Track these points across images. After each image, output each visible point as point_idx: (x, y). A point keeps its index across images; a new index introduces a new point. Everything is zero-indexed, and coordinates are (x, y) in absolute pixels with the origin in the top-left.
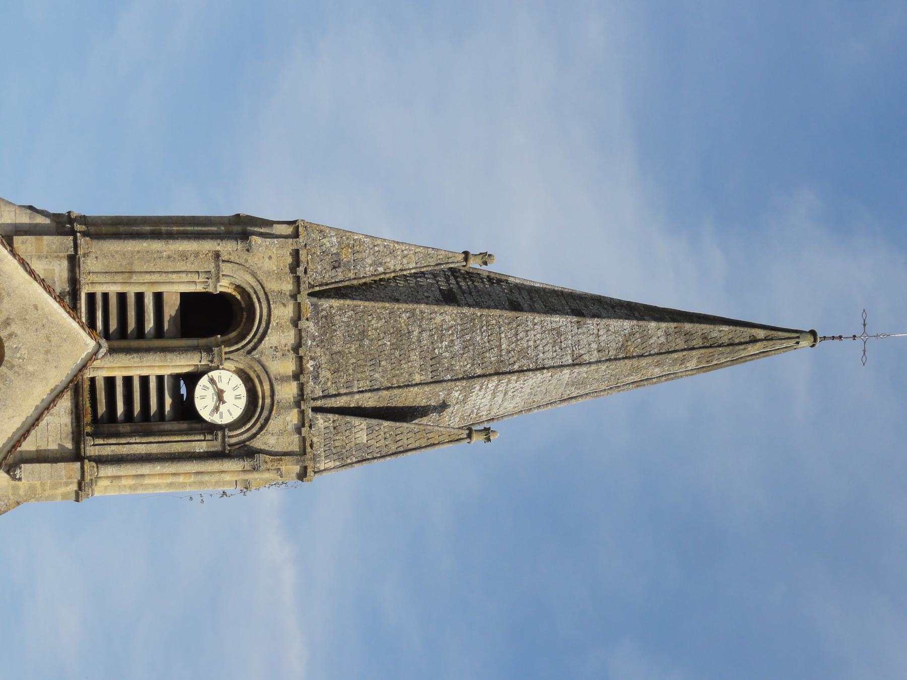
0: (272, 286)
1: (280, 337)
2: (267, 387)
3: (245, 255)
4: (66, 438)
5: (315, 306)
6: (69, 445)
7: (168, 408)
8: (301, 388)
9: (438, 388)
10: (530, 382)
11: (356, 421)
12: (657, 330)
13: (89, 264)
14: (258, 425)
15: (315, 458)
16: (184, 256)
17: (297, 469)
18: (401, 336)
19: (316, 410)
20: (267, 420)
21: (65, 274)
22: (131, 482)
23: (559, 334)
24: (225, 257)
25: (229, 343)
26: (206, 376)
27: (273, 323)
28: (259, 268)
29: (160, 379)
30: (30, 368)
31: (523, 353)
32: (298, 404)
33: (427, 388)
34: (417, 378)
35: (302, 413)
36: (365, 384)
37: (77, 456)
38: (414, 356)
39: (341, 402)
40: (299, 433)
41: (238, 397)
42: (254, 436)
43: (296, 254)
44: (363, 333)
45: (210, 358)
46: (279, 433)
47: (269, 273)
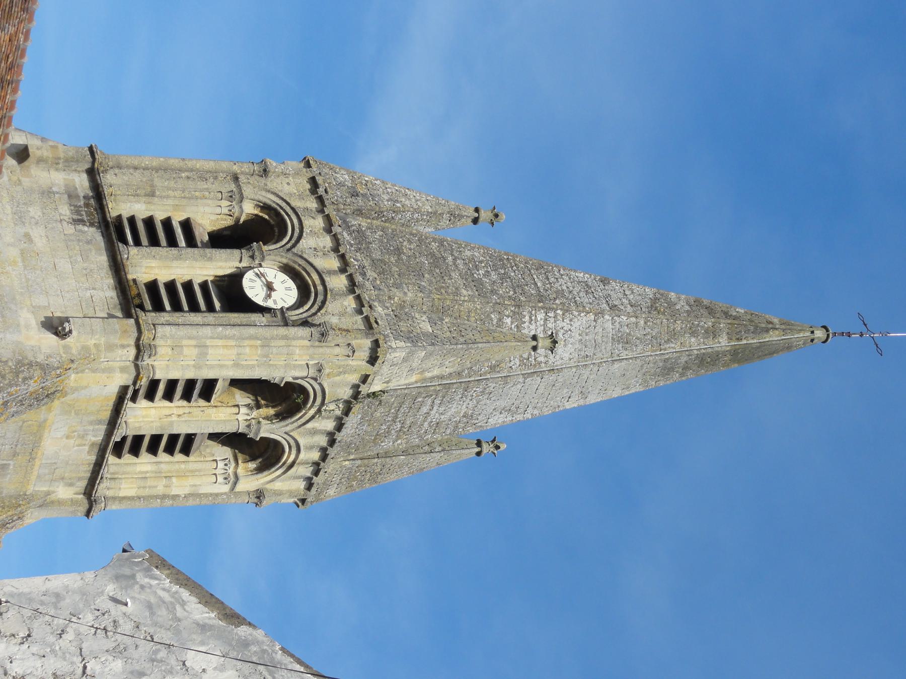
0: (319, 263)
4: (115, 308)
14: (316, 307)
20: (324, 302)
27: (306, 230)
29: (204, 286)
40: (361, 313)
42: (315, 314)
43: (313, 181)
45: (251, 253)
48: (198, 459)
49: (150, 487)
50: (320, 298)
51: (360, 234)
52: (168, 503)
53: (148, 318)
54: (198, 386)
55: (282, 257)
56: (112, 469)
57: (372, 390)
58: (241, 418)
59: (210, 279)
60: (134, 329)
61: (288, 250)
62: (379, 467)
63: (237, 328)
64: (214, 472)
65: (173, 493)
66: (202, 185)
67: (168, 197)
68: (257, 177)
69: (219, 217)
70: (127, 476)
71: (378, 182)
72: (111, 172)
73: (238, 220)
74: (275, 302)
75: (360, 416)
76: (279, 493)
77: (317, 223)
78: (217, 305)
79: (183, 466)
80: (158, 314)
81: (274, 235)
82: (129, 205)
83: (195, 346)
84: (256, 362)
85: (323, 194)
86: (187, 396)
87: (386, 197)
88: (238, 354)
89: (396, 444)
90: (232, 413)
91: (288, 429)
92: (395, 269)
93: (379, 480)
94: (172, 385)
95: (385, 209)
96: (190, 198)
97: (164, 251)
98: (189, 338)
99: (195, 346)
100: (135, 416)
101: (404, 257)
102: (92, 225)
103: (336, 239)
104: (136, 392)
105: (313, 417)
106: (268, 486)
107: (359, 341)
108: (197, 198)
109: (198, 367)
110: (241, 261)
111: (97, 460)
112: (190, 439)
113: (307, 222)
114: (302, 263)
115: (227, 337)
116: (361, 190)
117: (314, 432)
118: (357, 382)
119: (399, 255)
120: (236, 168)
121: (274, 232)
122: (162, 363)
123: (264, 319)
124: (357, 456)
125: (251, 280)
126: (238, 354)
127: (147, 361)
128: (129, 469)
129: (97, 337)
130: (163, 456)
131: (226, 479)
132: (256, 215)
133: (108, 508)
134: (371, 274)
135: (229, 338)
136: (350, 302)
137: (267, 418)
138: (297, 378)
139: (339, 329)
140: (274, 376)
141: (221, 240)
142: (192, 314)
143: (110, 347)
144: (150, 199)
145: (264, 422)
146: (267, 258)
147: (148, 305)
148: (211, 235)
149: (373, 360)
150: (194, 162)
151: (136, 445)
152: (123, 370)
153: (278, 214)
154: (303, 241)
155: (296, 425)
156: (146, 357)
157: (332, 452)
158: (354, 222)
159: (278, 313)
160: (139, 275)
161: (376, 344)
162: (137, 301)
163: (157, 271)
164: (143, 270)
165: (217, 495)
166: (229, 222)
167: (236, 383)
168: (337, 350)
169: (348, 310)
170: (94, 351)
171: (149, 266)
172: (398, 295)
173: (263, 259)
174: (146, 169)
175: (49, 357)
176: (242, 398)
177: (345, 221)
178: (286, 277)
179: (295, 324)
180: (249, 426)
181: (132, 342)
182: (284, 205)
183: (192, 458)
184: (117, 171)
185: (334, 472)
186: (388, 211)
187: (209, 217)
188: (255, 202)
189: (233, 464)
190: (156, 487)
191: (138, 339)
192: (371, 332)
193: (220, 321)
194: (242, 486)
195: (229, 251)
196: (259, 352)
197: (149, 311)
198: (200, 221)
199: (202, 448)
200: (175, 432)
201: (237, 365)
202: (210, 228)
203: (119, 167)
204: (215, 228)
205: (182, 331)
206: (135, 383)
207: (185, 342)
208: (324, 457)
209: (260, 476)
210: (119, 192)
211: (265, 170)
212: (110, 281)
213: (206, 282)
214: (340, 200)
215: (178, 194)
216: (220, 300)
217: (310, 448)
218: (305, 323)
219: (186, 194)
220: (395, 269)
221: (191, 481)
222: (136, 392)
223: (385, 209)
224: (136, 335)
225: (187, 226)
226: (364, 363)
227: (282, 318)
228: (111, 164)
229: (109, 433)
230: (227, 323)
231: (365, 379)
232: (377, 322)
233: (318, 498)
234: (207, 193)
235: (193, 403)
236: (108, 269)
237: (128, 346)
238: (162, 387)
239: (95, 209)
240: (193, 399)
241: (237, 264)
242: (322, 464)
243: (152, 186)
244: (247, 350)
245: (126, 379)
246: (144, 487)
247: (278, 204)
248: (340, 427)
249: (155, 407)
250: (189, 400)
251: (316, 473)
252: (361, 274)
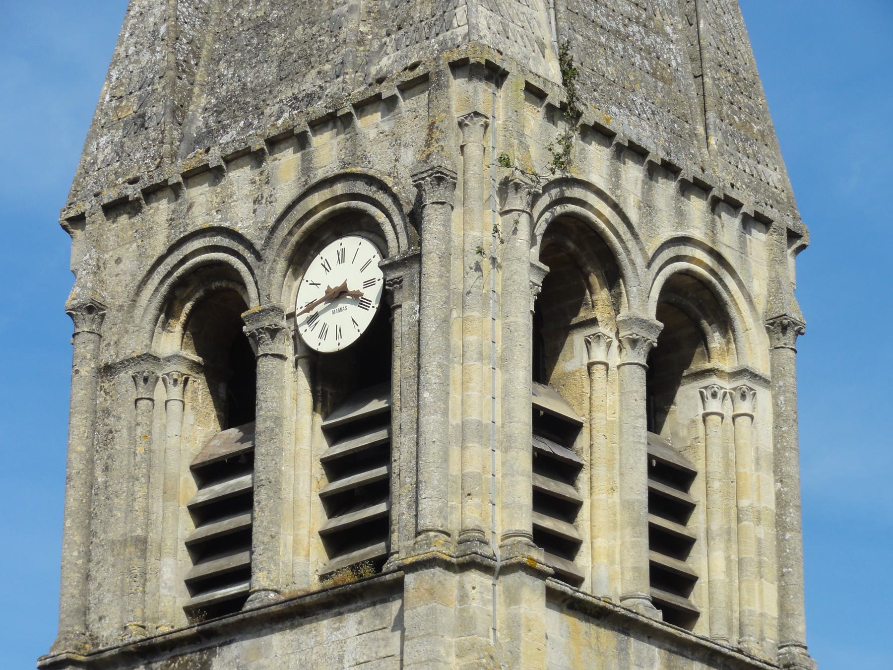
0: (286, 190)
4: (381, 616)
14: (381, 196)
20: (371, 180)
26: (301, 330)
27: (216, 220)
29: (334, 434)
40: (393, 100)
42: (395, 198)
43: (112, 209)
45: (266, 336)
48: (701, 453)
49: (760, 553)
50: (360, 187)
51: (225, 109)
52: (793, 516)
53: (402, 545)
54: (548, 446)
55: (272, 270)
56: (720, 631)
57: (557, 78)
58: (615, 359)
59: (319, 421)
60: (426, 574)
61: (259, 257)
62: (722, 74)
63: (425, 360)
64: (728, 420)
65: (772, 506)
66: (121, 441)
67: (147, 511)
68: (105, 327)
69: (188, 407)
70: (736, 601)
71: (114, 74)
72: (95, 627)
73: (194, 366)
74: (369, 283)
75: (614, 109)
76: (776, 286)
77: (202, 199)
78: (375, 405)
79: (716, 485)
80: (395, 527)
81: (228, 290)
82: (164, 591)
83: (463, 448)
84: (498, 322)
85: (139, 187)
86: (568, 471)
87: (146, 56)
88: (481, 357)
89: (674, 37)
90: (605, 379)
91: (640, 261)
92: (299, 33)
93: (750, 76)
94: (544, 502)
95: (171, 58)
96: (150, 466)
97: (261, 520)
98: (446, 459)
99: (463, 448)
100: (611, 579)
101: (275, 14)
103: (233, 159)
104: (560, 575)
105: (615, 207)
106: (761, 307)
107: (454, 104)
108: (149, 451)
109: (507, 445)
110: (282, 357)
111: (702, 660)
112: (660, 469)
113: (200, 219)
114: (286, 227)
115: (445, 381)
116: (131, 107)
117: (647, 206)
118: (542, 110)
119: (270, 25)
120: (86, 370)
121: (220, 290)
122: (498, 518)
123: (405, 306)
124: (699, 119)
125: (323, 333)
126: (481, 357)
127: (495, 549)
128: (720, 596)
129: (442, 652)
130: (695, 526)
131: (743, 396)
132: (185, 327)
133: (803, 640)
134: (309, 83)
135: (447, 377)
136: (370, 124)
137: (616, 306)
138: (533, 237)
139: (428, 145)
140: (527, 284)
141: (237, 402)
142: (395, 455)
143: (465, 624)
144: (152, 548)
145: (624, 312)
146: (274, 302)
147: (376, 549)
148: (227, 422)
149: (495, 75)
150: (73, 456)
151: (671, 581)
152: (512, 599)
153: (183, 283)
154: (240, 228)
155: (631, 244)
156: (486, 551)
157: (690, 171)
158: (198, 121)
159: (394, 275)
160: (312, 569)
161: (459, 67)
162: (367, 571)
163: (303, 532)
164: (301, 559)
165: (777, 415)
166: (199, 385)
167: (541, 372)
168: (473, 150)
169: (386, 127)
170: (472, 658)
171: (292, 549)
172: (353, 25)
173: (276, 310)
174: (88, 557)
176: (574, 355)
177: (198, 141)
178: (317, 263)
179: (416, 240)
180: (634, 343)
181: (453, 579)
182: (162, 270)
183: (698, 466)
184: (93, 617)
185: (732, 168)
186: (176, 51)
187: (190, 426)
188: (158, 329)
189: (714, 380)
190: (759, 541)
191: (448, 566)
192: (433, 78)
193: (410, 397)
194: (760, 363)
195: (260, 382)
196: (476, 314)
197: (388, 547)
198: (199, 445)
199: (678, 446)
200: (644, 497)
201: (504, 362)
202: (214, 425)
203: (85, 611)
204: (213, 415)
205: (432, 475)
206: (541, 575)
207: (455, 469)
208: (700, 187)
209: (738, 324)
210: (138, 612)
211: (90, 309)
212: (324, 628)
213: (326, 430)
214: (152, 151)
215: (140, 491)
216: (367, 400)
217: (681, 215)
218: (415, 219)
219: (141, 472)
220: (299, 33)
221: (748, 468)
222: (560, 575)
223: (171, 58)
224: (438, 571)
225: (206, 472)
226: (501, 93)
227: (403, 267)
228: (78, 629)
229: (646, 632)
230: (414, 383)
231: (535, 93)
232: (414, 67)
233: (790, 206)
234: (139, 430)
235: (584, 459)
236: (297, 631)
237: (462, 587)
238: (549, 523)
239: (174, 659)
240: (576, 459)
241: (289, 364)
242: (715, 192)
243: (124, 543)
244: (472, 339)
245: (531, 596)
246: (760, 564)
247: (162, 282)
248: (637, 152)
249: (592, 538)
250: (578, 467)
251: (734, 205)
252: (309, 104)
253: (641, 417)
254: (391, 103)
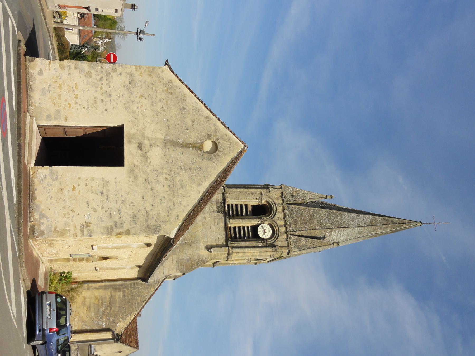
0: (276, 201)
1: (279, 215)
2: (277, 228)
3: (268, 193)
5: (288, 207)
6: (225, 243)
7: (250, 235)
8: (286, 228)
9: (323, 231)
10: (347, 231)
11: (302, 238)
12: (379, 219)
13: (227, 195)
15: (292, 248)
16: (252, 193)
17: (287, 251)
18: (312, 217)
19: (291, 235)
20: (278, 237)
21: (222, 198)
22: (242, 254)
23: (353, 218)
24: (263, 194)
25: (266, 217)
27: (277, 211)
28: (273, 196)
29: (248, 227)
30: (225, 152)
31: (344, 223)
32: (286, 233)
33: (320, 231)
34: (317, 228)
35: (287, 235)
36: (303, 229)
37: (227, 246)
38: (316, 222)
39: (297, 233)
41: (269, 231)
43: (282, 193)
44: (302, 215)
46: (281, 241)
47: (275, 198)
102: (221, 213)
116: (295, 194)
143: (221, 255)
175: (206, 258)
253: (132, 137)
254: (287, 240)
